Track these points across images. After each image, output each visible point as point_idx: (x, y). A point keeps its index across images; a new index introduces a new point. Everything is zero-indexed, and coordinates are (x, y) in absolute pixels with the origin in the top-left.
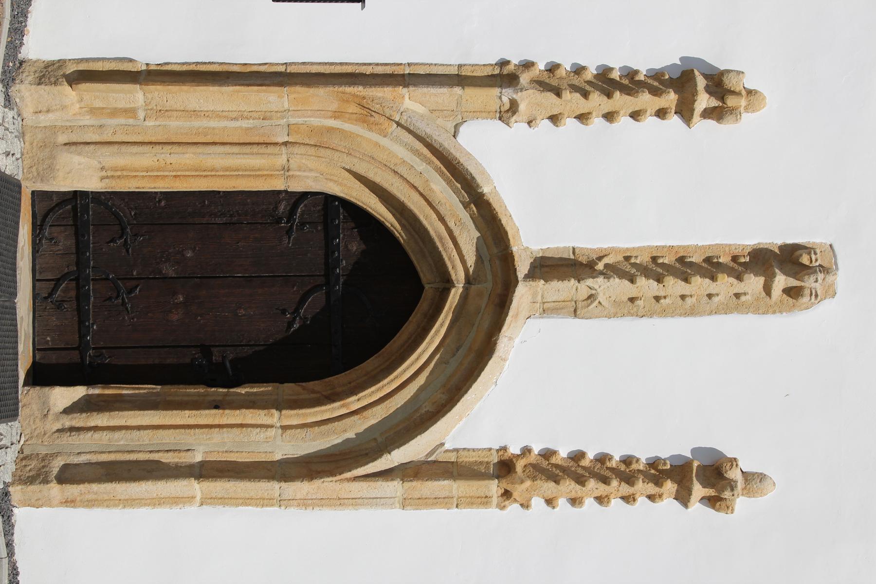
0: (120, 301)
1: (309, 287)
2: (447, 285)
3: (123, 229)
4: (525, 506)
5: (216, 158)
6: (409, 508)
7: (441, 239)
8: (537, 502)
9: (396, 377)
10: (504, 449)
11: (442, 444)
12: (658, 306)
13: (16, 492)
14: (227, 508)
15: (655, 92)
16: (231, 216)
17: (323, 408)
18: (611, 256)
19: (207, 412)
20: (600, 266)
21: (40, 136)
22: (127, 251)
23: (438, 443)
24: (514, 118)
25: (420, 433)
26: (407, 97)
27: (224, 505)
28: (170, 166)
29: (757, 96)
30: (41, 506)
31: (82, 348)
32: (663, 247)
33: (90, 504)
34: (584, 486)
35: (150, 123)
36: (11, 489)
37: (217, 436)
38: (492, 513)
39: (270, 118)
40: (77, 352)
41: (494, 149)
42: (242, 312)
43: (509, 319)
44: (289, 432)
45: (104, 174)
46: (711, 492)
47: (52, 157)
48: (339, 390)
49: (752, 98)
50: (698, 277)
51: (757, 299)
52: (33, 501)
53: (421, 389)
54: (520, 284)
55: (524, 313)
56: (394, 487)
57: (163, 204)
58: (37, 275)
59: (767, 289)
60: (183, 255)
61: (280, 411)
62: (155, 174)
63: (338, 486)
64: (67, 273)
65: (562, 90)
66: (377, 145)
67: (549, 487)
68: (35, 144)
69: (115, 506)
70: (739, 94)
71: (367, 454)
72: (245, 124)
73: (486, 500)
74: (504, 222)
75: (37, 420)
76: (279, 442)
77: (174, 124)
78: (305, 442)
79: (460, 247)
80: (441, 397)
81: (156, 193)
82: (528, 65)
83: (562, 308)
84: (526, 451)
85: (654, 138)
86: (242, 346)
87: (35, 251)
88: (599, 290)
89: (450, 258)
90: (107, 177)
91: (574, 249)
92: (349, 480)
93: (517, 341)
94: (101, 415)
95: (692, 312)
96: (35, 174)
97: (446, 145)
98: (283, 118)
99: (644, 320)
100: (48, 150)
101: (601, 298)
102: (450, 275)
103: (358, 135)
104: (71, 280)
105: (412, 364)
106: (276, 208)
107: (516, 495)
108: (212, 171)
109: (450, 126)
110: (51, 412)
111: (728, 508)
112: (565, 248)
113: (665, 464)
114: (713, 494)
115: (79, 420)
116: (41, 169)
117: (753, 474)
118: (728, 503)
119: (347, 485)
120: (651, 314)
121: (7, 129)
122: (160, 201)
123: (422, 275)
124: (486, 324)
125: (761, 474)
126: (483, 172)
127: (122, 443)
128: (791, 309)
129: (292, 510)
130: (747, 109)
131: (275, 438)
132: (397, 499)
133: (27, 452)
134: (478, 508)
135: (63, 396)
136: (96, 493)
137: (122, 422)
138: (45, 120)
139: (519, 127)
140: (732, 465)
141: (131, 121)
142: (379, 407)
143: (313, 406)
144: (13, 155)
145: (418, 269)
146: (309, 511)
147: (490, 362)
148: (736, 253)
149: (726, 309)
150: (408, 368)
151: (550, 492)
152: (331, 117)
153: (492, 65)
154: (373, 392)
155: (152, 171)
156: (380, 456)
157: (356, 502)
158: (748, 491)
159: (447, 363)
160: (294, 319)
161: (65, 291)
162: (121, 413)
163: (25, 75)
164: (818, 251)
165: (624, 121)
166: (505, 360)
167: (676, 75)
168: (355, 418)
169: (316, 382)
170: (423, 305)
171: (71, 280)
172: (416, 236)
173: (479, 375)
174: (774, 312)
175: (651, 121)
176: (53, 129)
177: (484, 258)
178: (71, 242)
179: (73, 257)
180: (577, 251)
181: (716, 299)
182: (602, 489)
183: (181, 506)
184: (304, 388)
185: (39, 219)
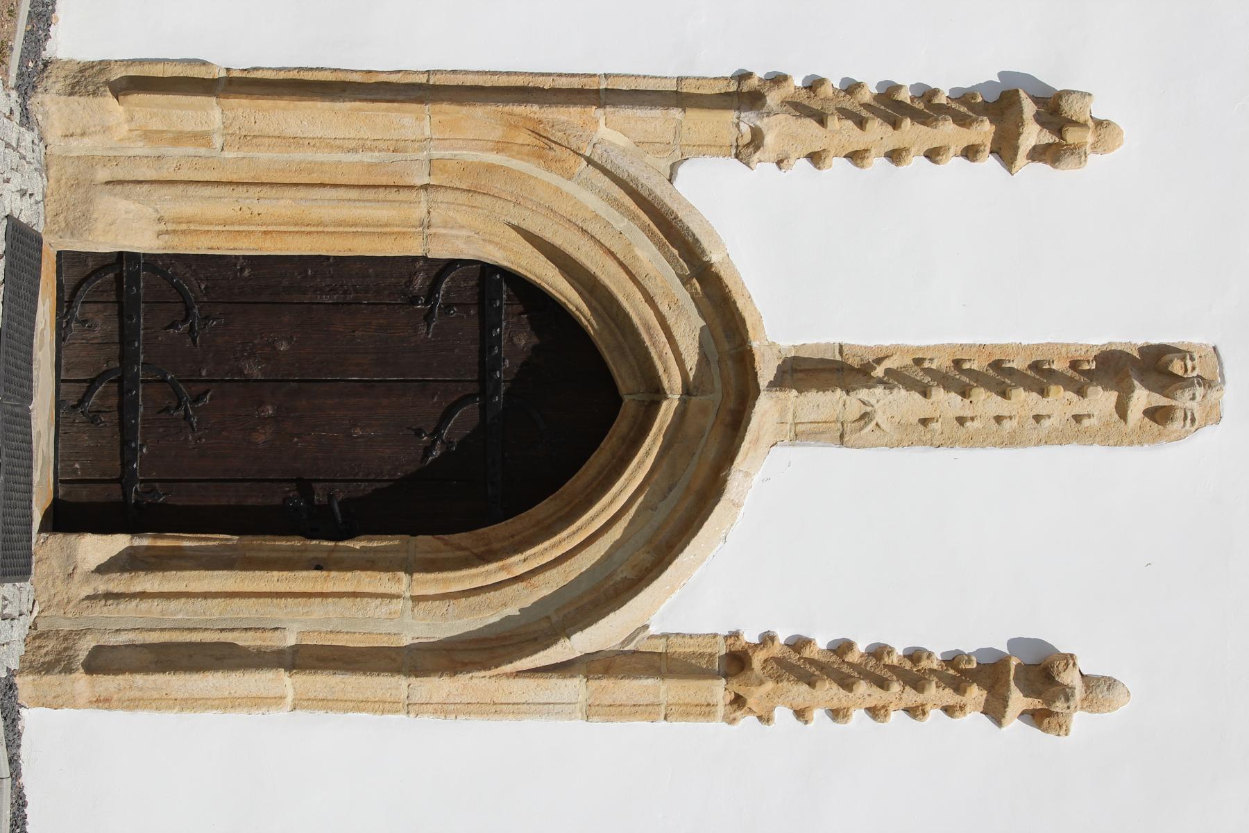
0: (182, 413)
1: (456, 398)
2: (656, 397)
4: (765, 719)
6: (595, 718)
7: (648, 328)
8: (783, 714)
10: (736, 635)
11: (646, 627)
12: (962, 432)
13: (25, 684)
14: (331, 714)
15: (962, 121)
16: (345, 292)
17: (474, 571)
18: (895, 357)
19: (305, 573)
20: (879, 372)
21: (70, 170)
22: (194, 340)
23: (640, 625)
26: (602, 122)
27: (327, 709)
28: (257, 218)
29: (1110, 128)
30: (61, 706)
31: (125, 479)
32: (971, 346)
33: (133, 704)
34: (851, 690)
35: (230, 154)
36: (17, 680)
37: (318, 609)
39: (404, 150)
42: (358, 431)
43: (745, 445)
44: (422, 605)
45: (162, 227)
47: (88, 201)
48: (496, 546)
50: (1100, 388)
51: (1107, 424)
52: (49, 698)
54: (762, 394)
55: (768, 439)
56: (574, 688)
57: (246, 273)
58: (63, 373)
59: (1122, 410)
60: (275, 348)
61: (411, 575)
62: (237, 228)
66: (558, 191)
68: (63, 182)
71: (536, 639)
72: (367, 157)
73: (708, 709)
75: (58, 582)
76: (408, 619)
77: (264, 156)
78: (447, 619)
79: (676, 342)
82: (778, 79)
83: (823, 433)
84: (767, 639)
85: (960, 189)
88: (876, 406)
90: (167, 232)
94: (151, 576)
95: (1011, 441)
96: (63, 225)
98: (422, 149)
99: (943, 452)
100: (81, 190)
101: (879, 418)
102: (660, 382)
103: (530, 177)
104: (111, 381)
105: (604, 509)
106: (410, 282)
107: (751, 702)
109: (664, 166)
110: (78, 571)
112: (828, 345)
113: (969, 661)
114: (1039, 707)
115: (118, 582)
116: (71, 218)
117: (1098, 678)
118: (1061, 719)
122: (242, 270)
123: (619, 382)
126: (712, 233)
127: (180, 617)
128: (1155, 439)
129: (426, 720)
130: (1094, 147)
131: (402, 613)
132: (578, 706)
134: (696, 720)
135: (97, 548)
137: (181, 587)
138: (79, 147)
139: (764, 169)
140: (1067, 664)
141: (203, 151)
142: (554, 571)
144: (31, 195)
145: (615, 373)
147: (717, 508)
148: (1077, 356)
150: (597, 515)
151: (800, 699)
152: (492, 150)
153: (726, 79)
154: (546, 549)
155: (232, 224)
156: (555, 642)
157: (518, 709)
158: (1090, 704)
159: (654, 508)
161: (103, 396)
163: (50, 81)
164: (1196, 356)
166: (738, 505)
168: (520, 586)
169: (464, 534)
170: (621, 425)
171: (111, 381)
172: (613, 325)
173: (700, 526)
174: (1131, 444)
176: (90, 161)
178: (113, 327)
179: (116, 349)
180: (845, 350)
181: (1046, 423)
183: (264, 709)
184: (446, 543)
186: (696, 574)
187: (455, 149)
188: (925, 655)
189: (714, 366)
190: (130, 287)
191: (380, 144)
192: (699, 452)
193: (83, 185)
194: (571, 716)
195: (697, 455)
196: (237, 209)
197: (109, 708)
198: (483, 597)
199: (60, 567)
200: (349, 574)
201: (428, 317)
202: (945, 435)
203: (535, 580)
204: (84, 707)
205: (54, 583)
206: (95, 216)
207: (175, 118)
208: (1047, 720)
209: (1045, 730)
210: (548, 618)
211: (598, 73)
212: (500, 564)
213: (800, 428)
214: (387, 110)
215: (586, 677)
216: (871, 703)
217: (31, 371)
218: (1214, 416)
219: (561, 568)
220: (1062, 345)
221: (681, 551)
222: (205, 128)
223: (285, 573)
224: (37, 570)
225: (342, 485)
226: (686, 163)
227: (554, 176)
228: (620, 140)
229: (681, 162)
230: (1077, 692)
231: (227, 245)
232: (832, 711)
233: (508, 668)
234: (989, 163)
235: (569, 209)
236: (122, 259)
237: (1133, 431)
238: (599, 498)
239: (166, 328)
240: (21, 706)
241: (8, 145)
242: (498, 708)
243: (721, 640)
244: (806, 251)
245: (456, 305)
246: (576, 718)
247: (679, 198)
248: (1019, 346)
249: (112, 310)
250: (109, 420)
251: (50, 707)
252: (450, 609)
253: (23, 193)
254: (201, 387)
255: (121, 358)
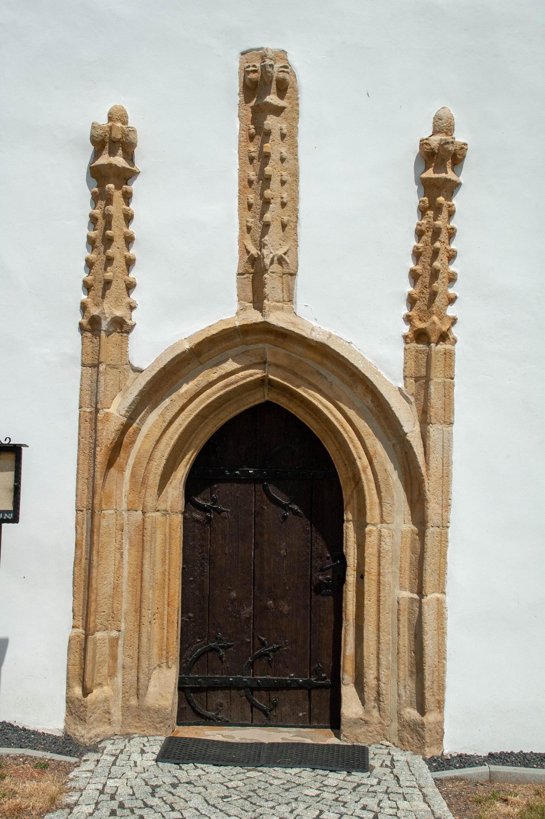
0: (271, 653)
1: (265, 496)
2: (267, 381)
3: (212, 649)
4: (454, 321)
5: (154, 570)
6: (452, 419)
7: (227, 386)
8: (451, 311)
9: (342, 426)
10: (405, 337)
11: (400, 388)
12: (290, 205)
13: (431, 752)
14: (448, 571)
15: (109, 201)
16: (203, 559)
17: (366, 488)
18: (245, 243)
19: (366, 585)
20: (254, 251)
21: (130, 720)
22: (230, 646)
23: (398, 393)
24: (127, 321)
25: (390, 408)
26: (107, 410)
27: (445, 574)
28: (160, 610)
29: (113, 113)
30: (443, 730)
31: (309, 687)
32: (239, 198)
33: (442, 688)
34: (439, 270)
35: (123, 626)
36: (428, 757)
37: (387, 578)
38: (458, 349)
39: (122, 525)
40: (313, 692)
41: (155, 337)
42: (283, 552)
43: (296, 331)
44: (385, 518)
45: (164, 665)
46: (449, 163)
47: (148, 710)
48: (350, 474)
49: (115, 117)
50: (265, 122)
51: (286, 119)
52: (438, 737)
53: (359, 412)
54: (266, 320)
55: (291, 317)
56: (434, 431)
57: (191, 615)
58: (247, 722)
59: (278, 111)
60: (234, 599)
61: (367, 524)
62: (165, 622)
63: (433, 478)
64: (246, 696)
65: (104, 280)
66: (146, 437)
67: (439, 301)
68: (137, 725)
69: (444, 666)
70: (111, 128)
71: (406, 453)
72: (126, 547)
73: (448, 354)
74: (214, 332)
75: (370, 729)
76: (393, 526)
77: (125, 606)
78: (394, 504)
79: (231, 374)
80: (360, 389)
81: (182, 621)
82: (84, 307)
83: (289, 285)
84: (408, 319)
85: (149, 204)
86: (311, 553)
87: (226, 723)
88: (274, 254)
89: (244, 379)
90: (167, 662)
91: (239, 274)
92: (428, 469)
93: (314, 324)
94: (366, 675)
95: (295, 175)
96: (162, 725)
97: (148, 378)
98: (121, 514)
99: (300, 216)
100: (142, 714)
101: (280, 252)
102: (258, 378)
103: (139, 452)
104: (252, 694)
105: (331, 413)
106: (197, 521)
107: (444, 329)
108: (165, 575)
109: (132, 375)
110: (363, 717)
111: (462, 148)
112: (238, 281)
113: (423, 202)
114: (450, 161)
115: (370, 694)
116: (158, 720)
117: (434, 126)
118: (458, 148)
119: (431, 471)
120: (296, 210)
121: (122, 752)
122: (189, 618)
123: (257, 402)
124: (301, 349)
125: (434, 119)
126: (172, 348)
127: (390, 658)
128: (296, 91)
129: (452, 517)
130: (125, 123)
131: (390, 529)
132: (444, 429)
133: (396, 740)
134: (454, 361)
135: (351, 706)
136: (433, 682)
137: (373, 657)
138: (117, 714)
139: (136, 317)
140: (426, 144)
141: (120, 642)
142: (367, 442)
143: (364, 496)
144: (144, 746)
145: (252, 405)
146: (453, 502)
147: (332, 347)
148: (245, 135)
149: (294, 146)
150: (334, 416)
151: (443, 300)
152: (123, 474)
153: (82, 338)
154: (354, 446)
155: (163, 624)
156: (408, 442)
157: (447, 463)
158: (449, 129)
159: (331, 384)
160: (291, 509)
161: (261, 698)
162: (365, 658)
163: (77, 734)
164: (247, 65)
165: (133, 229)
166: (330, 335)
167: (94, 182)
168: (375, 461)
169: (343, 493)
170: (283, 402)
171: (252, 694)
172: (225, 406)
173: (343, 357)
174: (297, 105)
175: (133, 207)
176: (126, 708)
177: (244, 350)
178: (220, 694)
179: (234, 692)
180: (241, 271)
181: (285, 154)
182: (443, 256)
183: (445, 610)
184: (349, 503)
185: (199, 720)
186: (370, 360)
187: (122, 496)
188: (419, 228)
189: (250, 347)
190: (199, 683)
191: (119, 538)
192: (299, 358)
193: (139, 714)
194: (450, 434)
195: (301, 358)
196: (154, 621)
197: (444, 701)
198: (381, 483)
199: (361, 728)
200: (367, 560)
201: (219, 512)
202: (292, 214)
203: (372, 453)
204: (443, 716)
205: (370, 732)
206: (157, 706)
207: (101, 659)
208: (459, 156)
209: (464, 157)
210: (394, 445)
211: (79, 412)
212: (362, 472)
213: (286, 299)
214: (99, 535)
215: (429, 424)
216: (446, 260)
217: (247, 744)
218: (282, 55)
219: (365, 438)
220: (239, 145)
221: (357, 368)
222: (107, 641)
223: (366, 597)
224: (363, 743)
225: (314, 561)
226: (132, 362)
227: (138, 438)
228: (118, 400)
229: (131, 365)
230: (443, 138)
231: (176, 628)
232: (450, 282)
233: (423, 470)
234: (135, 187)
235: (157, 430)
236: (182, 687)
237: (290, 103)
238: (324, 415)
239: (222, 662)
240: (442, 754)
241: (114, 764)
242: (445, 475)
243: (408, 346)
244: (182, 298)
245: (211, 495)
246: (452, 430)
247: (152, 367)
248: (240, 170)
249: (211, 693)
250: (274, 696)
251: (442, 736)
252: (387, 502)
253: (143, 752)
254: (256, 640)
255: (239, 689)
